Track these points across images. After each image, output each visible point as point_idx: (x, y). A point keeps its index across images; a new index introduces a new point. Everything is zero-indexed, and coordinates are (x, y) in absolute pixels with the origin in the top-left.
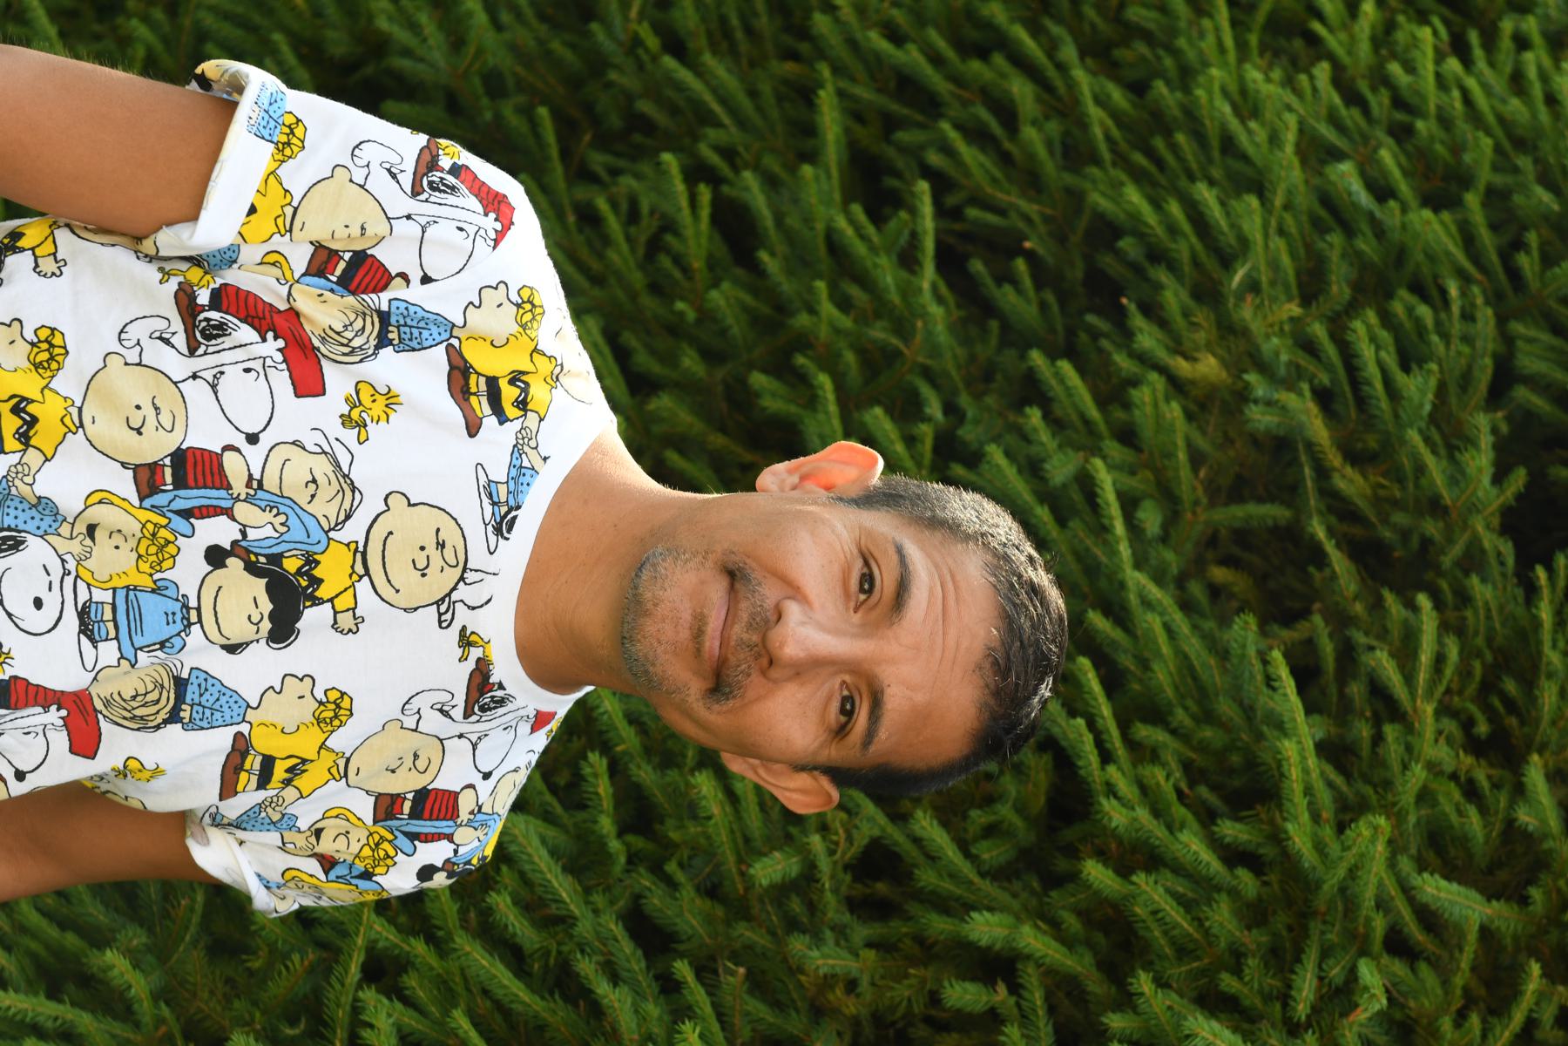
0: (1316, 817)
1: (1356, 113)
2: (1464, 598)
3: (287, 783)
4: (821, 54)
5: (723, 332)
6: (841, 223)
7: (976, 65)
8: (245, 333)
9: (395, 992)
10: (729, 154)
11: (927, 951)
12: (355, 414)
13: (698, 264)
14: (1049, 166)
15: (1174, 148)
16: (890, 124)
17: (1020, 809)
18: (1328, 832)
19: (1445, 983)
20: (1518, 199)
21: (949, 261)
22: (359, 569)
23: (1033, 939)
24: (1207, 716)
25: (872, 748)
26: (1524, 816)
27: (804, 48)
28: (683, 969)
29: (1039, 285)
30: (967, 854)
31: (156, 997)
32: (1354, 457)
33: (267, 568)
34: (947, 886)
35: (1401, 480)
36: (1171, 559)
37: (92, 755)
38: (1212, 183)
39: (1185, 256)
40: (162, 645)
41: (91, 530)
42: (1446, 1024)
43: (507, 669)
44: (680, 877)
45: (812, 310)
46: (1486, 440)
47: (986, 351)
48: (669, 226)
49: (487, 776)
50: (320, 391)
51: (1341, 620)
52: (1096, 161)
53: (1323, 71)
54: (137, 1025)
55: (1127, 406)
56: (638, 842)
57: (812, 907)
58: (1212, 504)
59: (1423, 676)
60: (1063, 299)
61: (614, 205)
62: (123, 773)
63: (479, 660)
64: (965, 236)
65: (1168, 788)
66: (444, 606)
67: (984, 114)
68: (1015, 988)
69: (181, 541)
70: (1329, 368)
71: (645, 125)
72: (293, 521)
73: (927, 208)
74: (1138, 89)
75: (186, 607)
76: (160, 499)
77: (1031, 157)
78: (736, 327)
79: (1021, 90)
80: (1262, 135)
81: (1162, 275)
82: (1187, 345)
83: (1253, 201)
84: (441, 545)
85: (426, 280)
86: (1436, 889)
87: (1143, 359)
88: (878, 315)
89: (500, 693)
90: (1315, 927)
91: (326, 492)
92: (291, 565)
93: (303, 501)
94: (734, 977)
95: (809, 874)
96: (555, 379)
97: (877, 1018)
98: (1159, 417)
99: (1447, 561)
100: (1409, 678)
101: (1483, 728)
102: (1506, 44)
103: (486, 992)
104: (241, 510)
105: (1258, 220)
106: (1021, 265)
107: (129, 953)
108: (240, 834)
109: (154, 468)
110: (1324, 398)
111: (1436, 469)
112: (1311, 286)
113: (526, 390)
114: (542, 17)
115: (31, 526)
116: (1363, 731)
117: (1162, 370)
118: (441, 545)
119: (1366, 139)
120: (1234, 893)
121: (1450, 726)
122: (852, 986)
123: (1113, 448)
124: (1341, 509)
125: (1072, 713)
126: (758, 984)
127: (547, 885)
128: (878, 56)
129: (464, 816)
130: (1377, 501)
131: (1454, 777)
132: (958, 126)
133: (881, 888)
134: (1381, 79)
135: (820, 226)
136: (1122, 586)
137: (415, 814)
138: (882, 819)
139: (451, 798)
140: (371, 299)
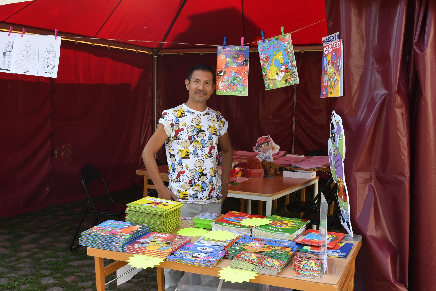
22: (198, 125)
25: (211, 81)
33: (198, 133)
40: (205, 141)
41: (196, 147)
43: (205, 112)
66: (200, 118)
69: (196, 140)
75: (203, 183)
84: (196, 118)
85: (172, 120)
92: (200, 174)
104: (194, 135)
109: (190, 142)
113: (182, 111)
115: (196, 152)
129: (217, 115)
139: (216, 116)
140: (174, 125)
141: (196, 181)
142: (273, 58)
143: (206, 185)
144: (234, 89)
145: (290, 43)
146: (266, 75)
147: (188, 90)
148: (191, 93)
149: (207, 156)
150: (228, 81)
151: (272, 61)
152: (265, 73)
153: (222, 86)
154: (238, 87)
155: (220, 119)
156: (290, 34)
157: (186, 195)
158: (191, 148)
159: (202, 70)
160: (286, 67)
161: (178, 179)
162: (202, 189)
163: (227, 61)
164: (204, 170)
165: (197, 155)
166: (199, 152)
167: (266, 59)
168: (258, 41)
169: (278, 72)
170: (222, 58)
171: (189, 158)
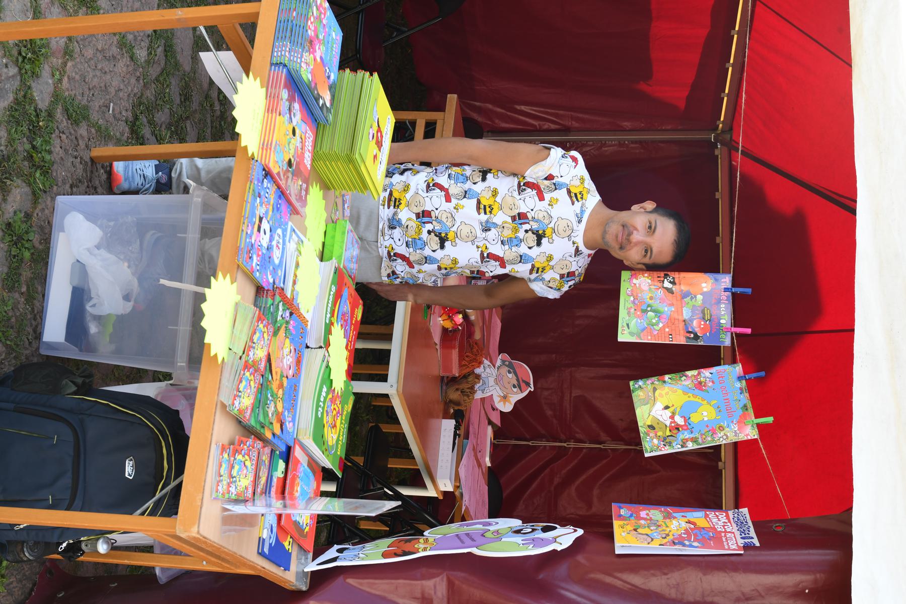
3: (542, 272)
8: (529, 190)
12: (456, 207)
22: (553, 232)
33: (438, 235)
41: (503, 227)
43: (582, 248)
49: (580, 267)
50: (450, 202)
63: (481, 251)
66: (569, 236)
72: (541, 224)
75: (424, 242)
76: (516, 222)
85: (561, 177)
89: (581, 252)
91: (546, 218)
92: (443, 235)
113: (582, 195)
118: (568, 226)
141: (429, 227)
142: (703, 400)
143: (418, 249)
144: (632, 310)
145: (736, 436)
146: (664, 382)
147: (632, 208)
148: (624, 215)
149: (484, 249)
150: (651, 298)
151: (695, 396)
152: (670, 381)
153: (640, 285)
154: (637, 321)
155: (567, 281)
156: (756, 437)
157: (397, 203)
158: (500, 218)
159: (675, 240)
160: (681, 426)
161: (433, 188)
162: (410, 240)
163: (695, 297)
165: (486, 230)
166: (493, 233)
167: (700, 383)
168: (741, 366)
169: (671, 409)
170: (704, 285)
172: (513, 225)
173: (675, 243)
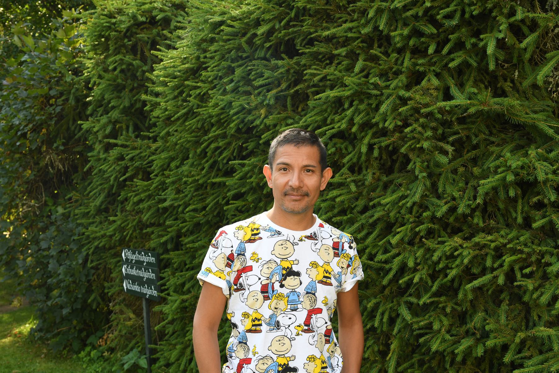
0: (344, 91)
1: (217, 86)
2: (305, 65)
4: (206, 182)
5: (256, 199)
6: (236, 177)
7: (208, 154)
8: (241, 280)
9: (375, 255)
10: (224, 198)
11: (368, 160)
13: (244, 203)
14: (227, 141)
15: (223, 118)
16: (219, 170)
17: (342, 144)
18: (347, 88)
19: (373, 68)
20: (233, 57)
21: (244, 158)
23: (366, 141)
24: (326, 111)
26: (344, 54)
27: (205, 185)
28: (371, 204)
29: (248, 142)
30: (350, 153)
31: (375, 298)
32: (279, 85)
34: (356, 156)
35: (283, 77)
36: (297, 117)
37: (322, 310)
38: (230, 111)
39: (243, 116)
41: (276, 308)
42: (381, 67)
43: (308, 232)
44: (354, 204)
45: (252, 182)
46: (276, 62)
47: (260, 152)
48: (237, 209)
51: (309, 87)
52: (225, 132)
53: (210, 92)
54: (381, 301)
55: (270, 126)
56: (348, 212)
57: (360, 181)
58: (288, 111)
59: (318, 72)
60: (250, 138)
61: (233, 219)
62: (326, 304)
64: (239, 156)
65: (339, 117)
67: (217, 152)
68: (375, 144)
70: (263, 90)
71: (219, 213)
73: (234, 162)
74: (213, 125)
76: (270, 296)
77: (225, 144)
78: (255, 196)
79: (213, 146)
80: (221, 103)
81: (246, 120)
82: (259, 115)
83: (233, 103)
84: (282, 245)
85: (232, 247)
86: (357, 69)
87: (261, 123)
88: (253, 171)
90: (364, 91)
92: (284, 272)
93: (272, 270)
94: (373, 195)
95: (354, 181)
96: (254, 223)
97: (380, 169)
98: (272, 120)
99: (298, 68)
100: (319, 75)
101: (328, 62)
102: (205, 60)
103: (375, 239)
105: (236, 103)
106: (244, 145)
107: (368, 303)
108: (343, 282)
109: (264, 297)
110: (268, 91)
111: (281, 70)
112: (249, 93)
113: (255, 229)
114: (199, 232)
116: (328, 83)
117: (263, 119)
118: (282, 245)
119: (222, 84)
120: (357, 105)
121: (327, 67)
122: (374, 174)
123: (277, 128)
124: (289, 87)
125: (325, 134)
126: (374, 190)
127: (356, 228)
128: (207, 172)
129: (339, 240)
130: (287, 81)
131: (336, 67)
132: (219, 157)
133: (356, 169)
134: (212, 82)
135: (237, 181)
136: (302, 126)
137: (338, 250)
138: (344, 168)
149: (300, 329)
158: (266, 312)
159: (295, 146)
164: (292, 359)
165: (278, 325)
166: (283, 320)
171: (260, 331)
172: (273, 299)
173: (298, 146)
